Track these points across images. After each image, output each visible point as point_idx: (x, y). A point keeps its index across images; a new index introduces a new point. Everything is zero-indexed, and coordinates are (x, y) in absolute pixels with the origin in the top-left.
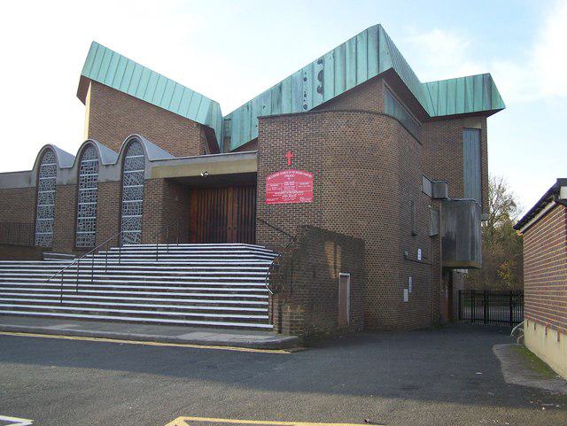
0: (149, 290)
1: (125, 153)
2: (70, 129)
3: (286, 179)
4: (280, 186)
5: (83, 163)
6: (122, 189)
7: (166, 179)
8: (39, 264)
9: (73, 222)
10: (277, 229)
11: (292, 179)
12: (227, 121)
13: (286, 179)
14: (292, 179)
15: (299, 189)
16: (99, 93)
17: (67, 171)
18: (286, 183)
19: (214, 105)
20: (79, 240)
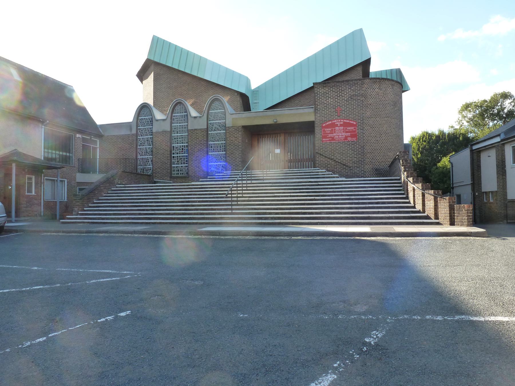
0: (99, 219)
1: (172, 112)
2: (144, 92)
3: (337, 126)
4: (332, 130)
5: (174, 116)
6: (207, 134)
7: (244, 127)
8: (180, 186)
9: (169, 158)
10: (332, 159)
11: (341, 125)
12: (256, 92)
13: (337, 126)
14: (341, 125)
15: (347, 132)
16: (164, 70)
17: (162, 121)
18: (337, 128)
19: (247, 81)
20: (174, 171)
